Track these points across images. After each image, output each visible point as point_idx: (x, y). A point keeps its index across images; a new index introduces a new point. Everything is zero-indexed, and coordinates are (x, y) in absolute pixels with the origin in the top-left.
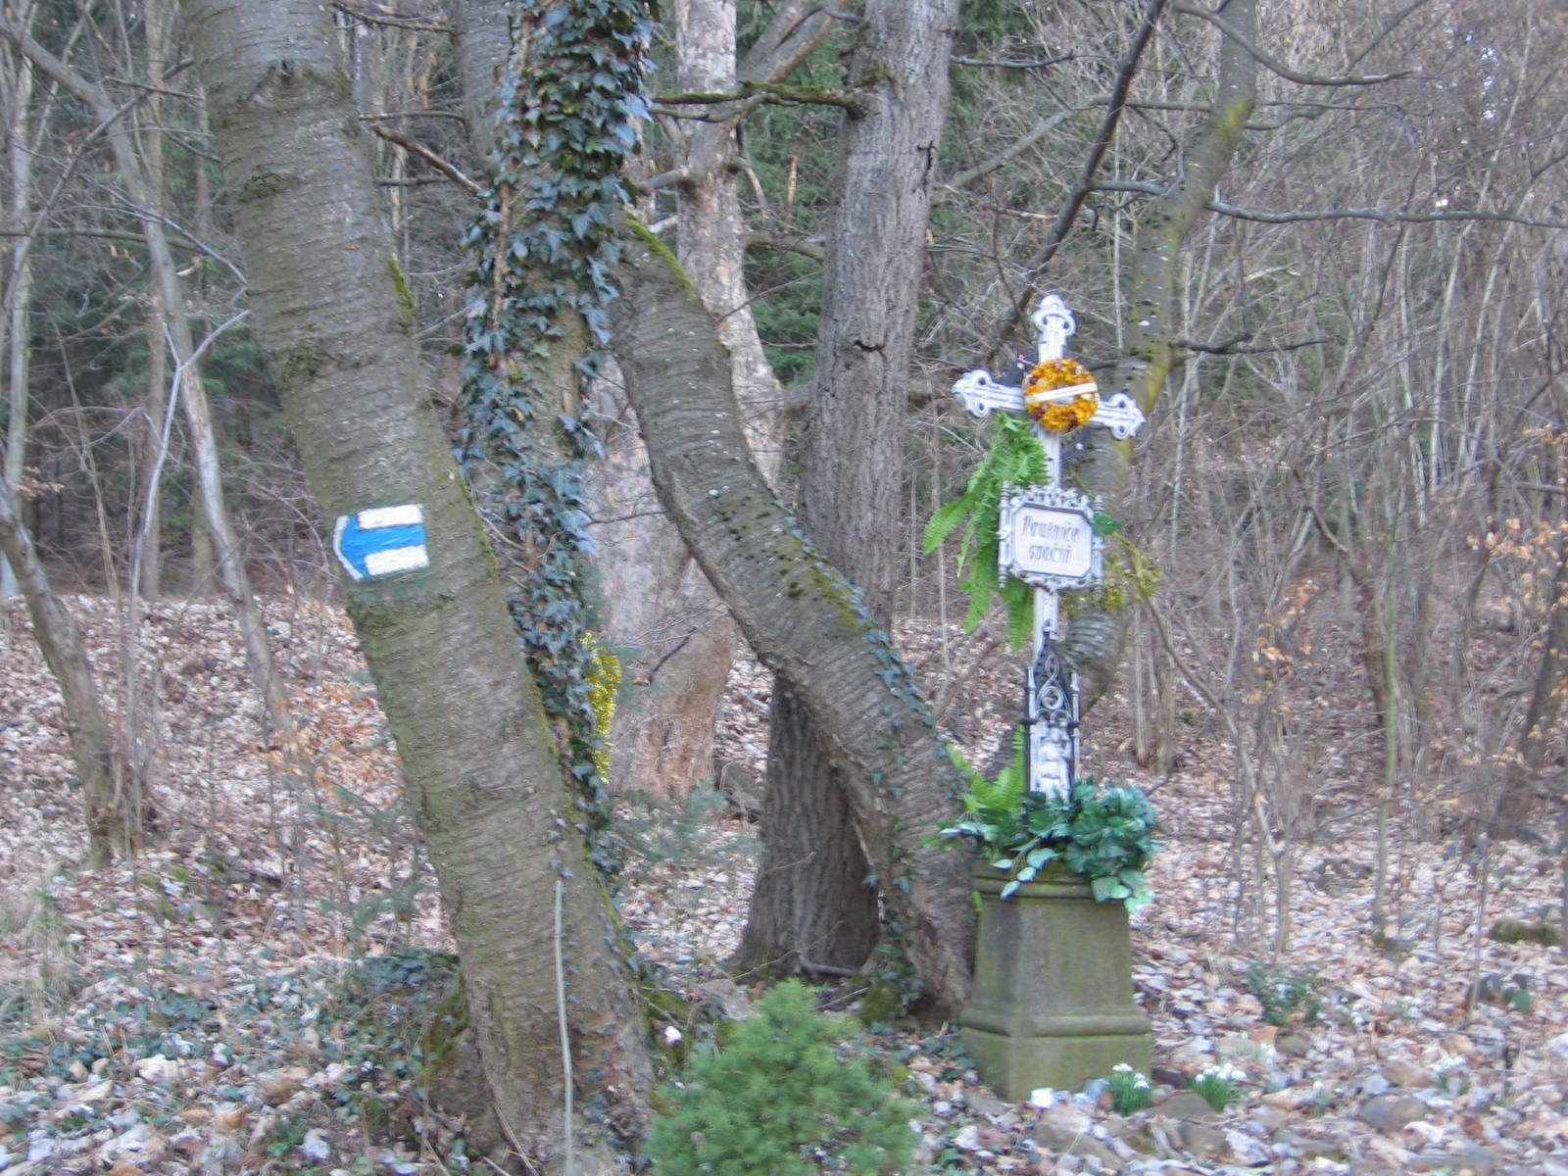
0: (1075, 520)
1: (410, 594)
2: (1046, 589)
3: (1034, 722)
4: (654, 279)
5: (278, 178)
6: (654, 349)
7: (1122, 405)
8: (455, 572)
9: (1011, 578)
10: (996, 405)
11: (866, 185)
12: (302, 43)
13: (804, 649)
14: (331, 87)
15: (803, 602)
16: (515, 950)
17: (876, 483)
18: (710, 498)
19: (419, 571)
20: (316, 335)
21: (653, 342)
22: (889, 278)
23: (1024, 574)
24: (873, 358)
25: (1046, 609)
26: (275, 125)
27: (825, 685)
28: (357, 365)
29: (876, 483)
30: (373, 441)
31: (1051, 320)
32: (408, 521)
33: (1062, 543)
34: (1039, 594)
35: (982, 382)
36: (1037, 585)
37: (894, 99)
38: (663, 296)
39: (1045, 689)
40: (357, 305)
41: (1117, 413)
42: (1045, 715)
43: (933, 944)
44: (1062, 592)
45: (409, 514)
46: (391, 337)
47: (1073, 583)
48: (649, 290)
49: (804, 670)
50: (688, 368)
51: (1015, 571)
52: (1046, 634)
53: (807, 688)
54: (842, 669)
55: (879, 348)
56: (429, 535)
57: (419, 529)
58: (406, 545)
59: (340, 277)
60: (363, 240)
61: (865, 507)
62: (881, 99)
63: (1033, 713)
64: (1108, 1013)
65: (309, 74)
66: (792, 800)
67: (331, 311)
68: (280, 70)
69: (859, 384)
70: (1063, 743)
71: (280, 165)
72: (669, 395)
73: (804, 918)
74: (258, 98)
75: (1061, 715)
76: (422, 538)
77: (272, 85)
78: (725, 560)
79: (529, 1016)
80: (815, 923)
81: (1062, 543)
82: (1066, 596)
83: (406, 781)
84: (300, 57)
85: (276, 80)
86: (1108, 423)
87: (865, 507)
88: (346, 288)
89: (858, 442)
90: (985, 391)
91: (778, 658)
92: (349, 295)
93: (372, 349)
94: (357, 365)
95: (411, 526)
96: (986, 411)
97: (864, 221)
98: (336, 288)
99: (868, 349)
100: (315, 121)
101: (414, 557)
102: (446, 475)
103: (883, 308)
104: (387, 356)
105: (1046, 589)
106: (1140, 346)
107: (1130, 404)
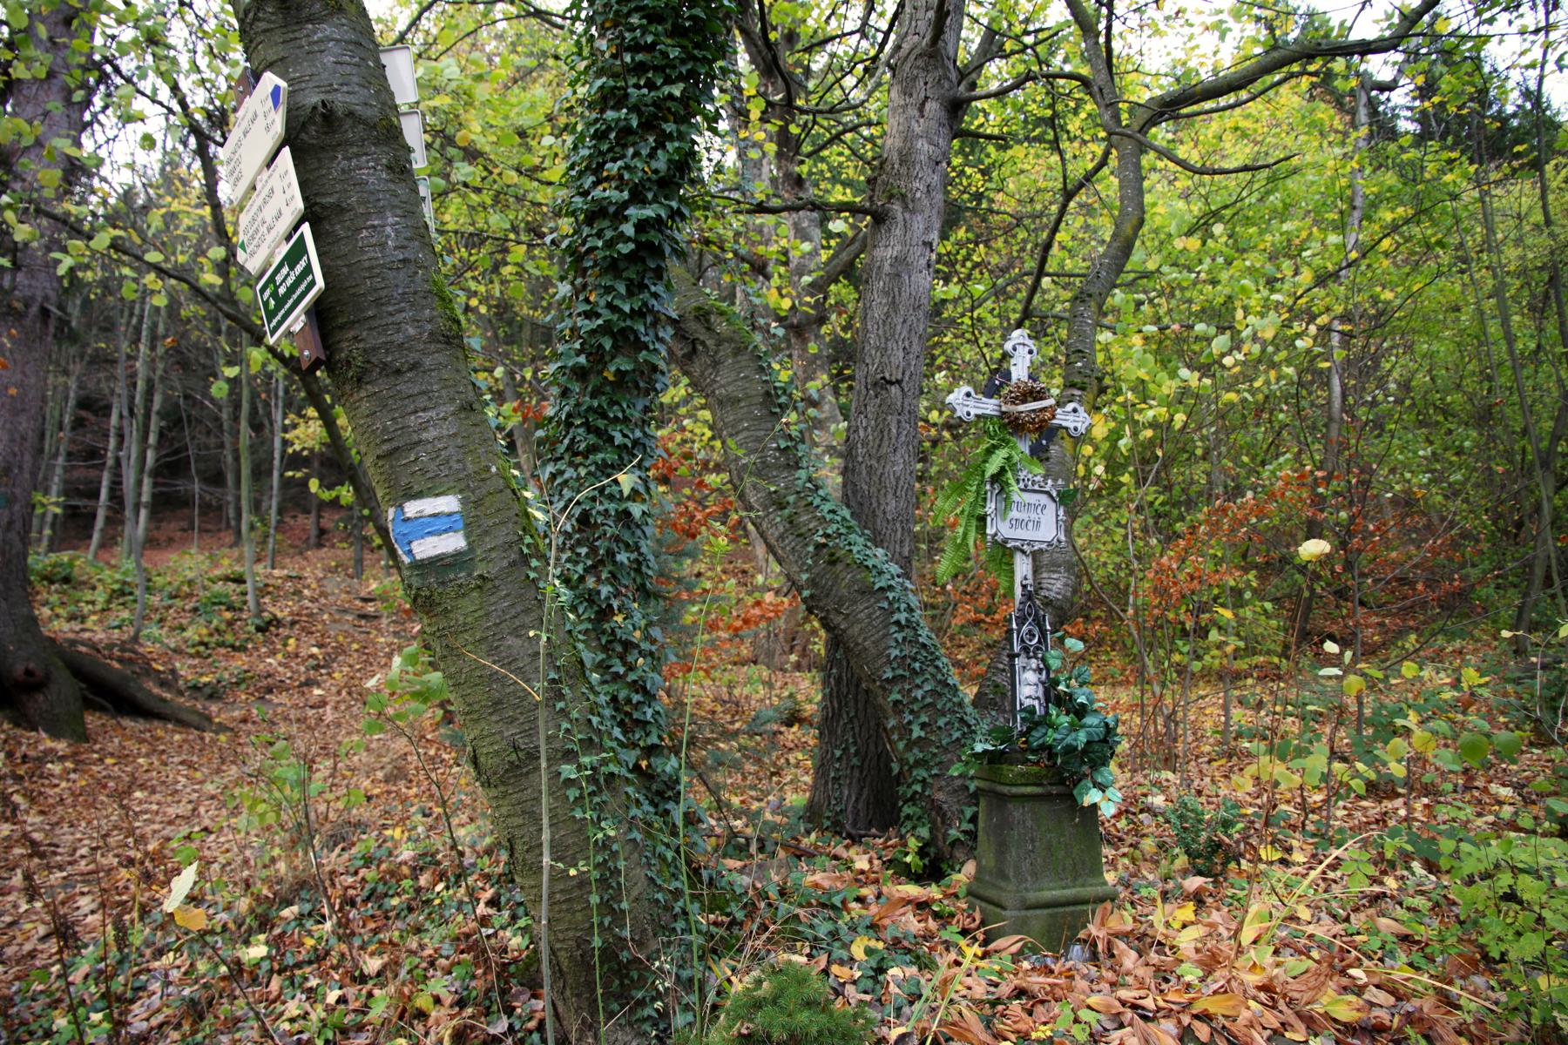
0: (1044, 499)
1: (452, 576)
2: (1024, 552)
3: (1018, 655)
4: (731, 340)
5: (323, 207)
6: (730, 389)
7: (1075, 411)
8: (493, 555)
9: (995, 542)
10: (979, 412)
11: (887, 268)
12: (345, 88)
13: (841, 602)
14: (374, 127)
15: (840, 567)
16: (562, 891)
17: (898, 479)
18: (770, 493)
19: (458, 554)
20: (361, 345)
21: (729, 384)
22: (905, 333)
23: (1006, 541)
24: (894, 390)
25: (1023, 567)
26: (320, 160)
27: (856, 629)
28: (398, 372)
29: (898, 479)
30: (415, 437)
31: (1020, 348)
32: (446, 509)
33: (1033, 516)
34: (1018, 557)
35: (968, 395)
36: (1017, 548)
37: (906, 208)
38: (737, 352)
39: (1025, 628)
40: (399, 317)
41: (1071, 417)
42: (1026, 649)
43: (943, 822)
44: (1034, 554)
45: (448, 503)
46: (433, 347)
47: (1044, 546)
48: (726, 349)
49: (841, 618)
50: (755, 401)
51: (999, 538)
52: (1024, 587)
53: (844, 631)
54: (869, 616)
55: (899, 382)
56: (471, 523)
57: (457, 517)
58: (446, 531)
59: (383, 293)
60: (404, 261)
61: (890, 496)
62: (897, 207)
63: (1016, 649)
64: (1083, 886)
65: (351, 114)
66: (840, 708)
67: (374, 323)
68: (321, 109)
69: (884, 408)
70: (1039, 670)
71: (323, 195)
72: (741, 420)
73: (849, 796)
74: (304, 136)
75: (1038, 649)
76: (461, 525)
77: (315, 123)
78: (782, 537)
79: (578, 947)
80: (857, 800)
81: (1033, 516)
82: (1036, 555)
83: (867, 591)
84: (340, 101)
85: (318, 119)
86: (1064, 424)
87: (890, 496)
88: (388, 303)
89: (884, 450)
90: (971, 402)
91: (822, 609)
92: (390, 309)
93: (413, 357)
94: (398, 372)
95: (450, 515)
96: (972, 417)
97: (887, 294)
98: (378, 302)
99: (891, 383)
100: (358, 156)
101: (453, 543)
102: (488, 469)
103: (901, 354)
104: (427, 361)
105: (1024, 552)
106: (1078, 380)
107: (1081, 409)
